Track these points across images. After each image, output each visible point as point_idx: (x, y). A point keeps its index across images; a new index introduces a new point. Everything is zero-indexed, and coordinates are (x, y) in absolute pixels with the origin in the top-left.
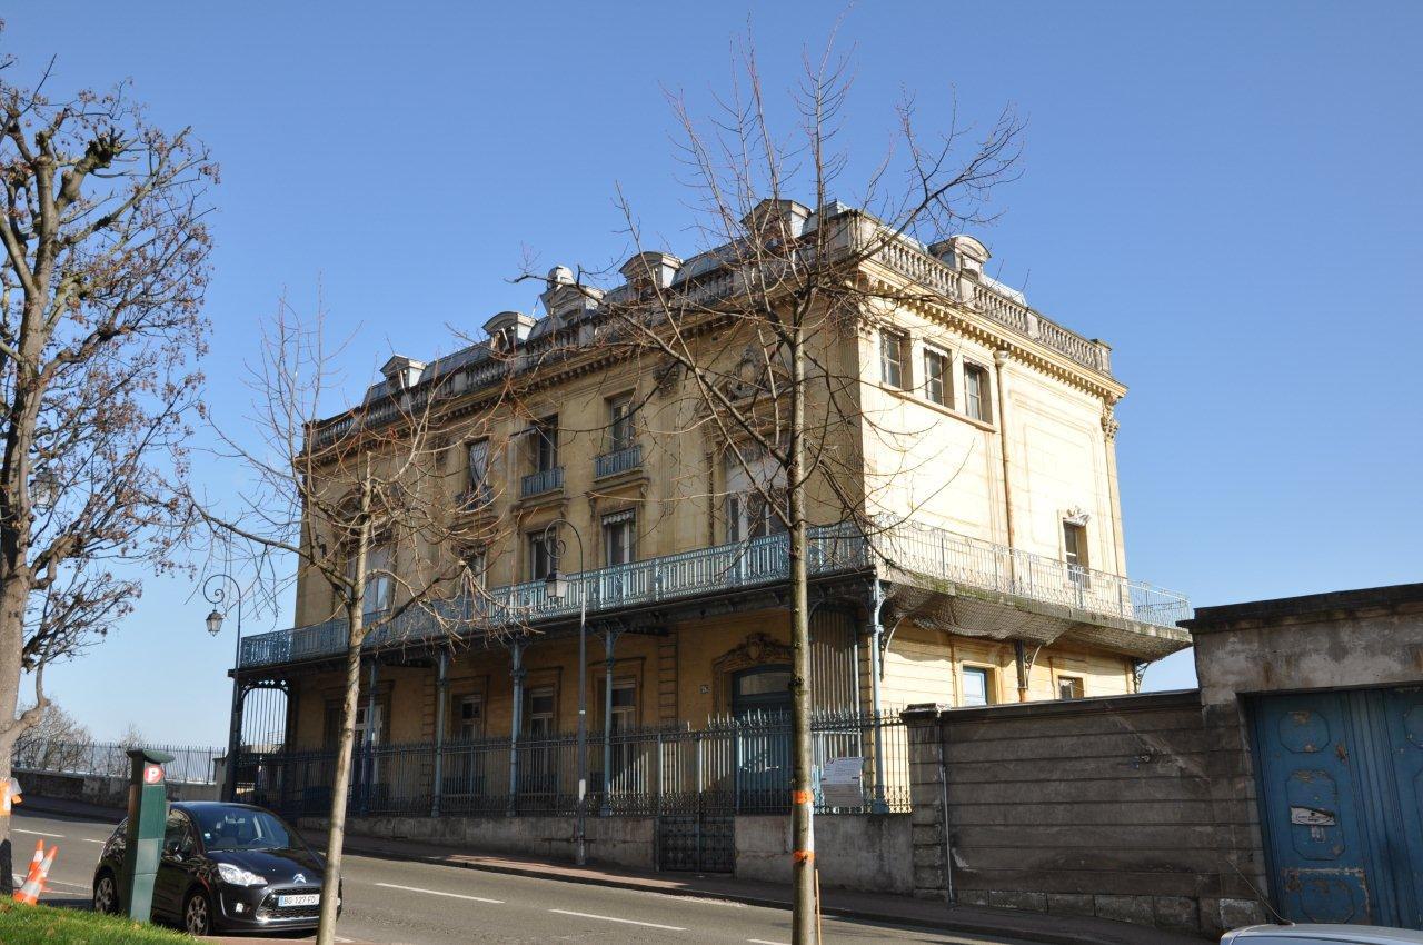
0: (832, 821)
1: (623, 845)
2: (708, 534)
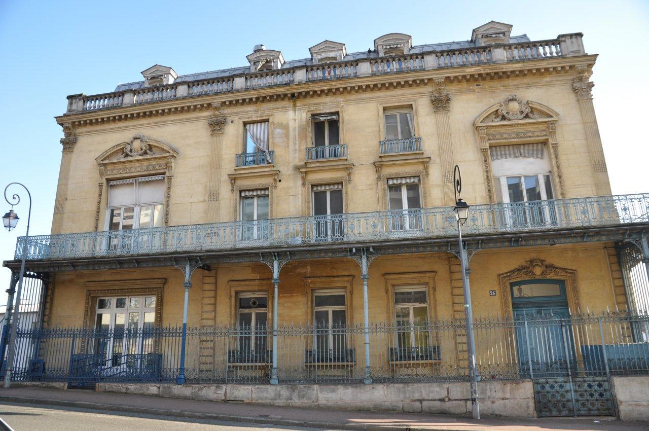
1: (503, 402)
2: (488, 197)
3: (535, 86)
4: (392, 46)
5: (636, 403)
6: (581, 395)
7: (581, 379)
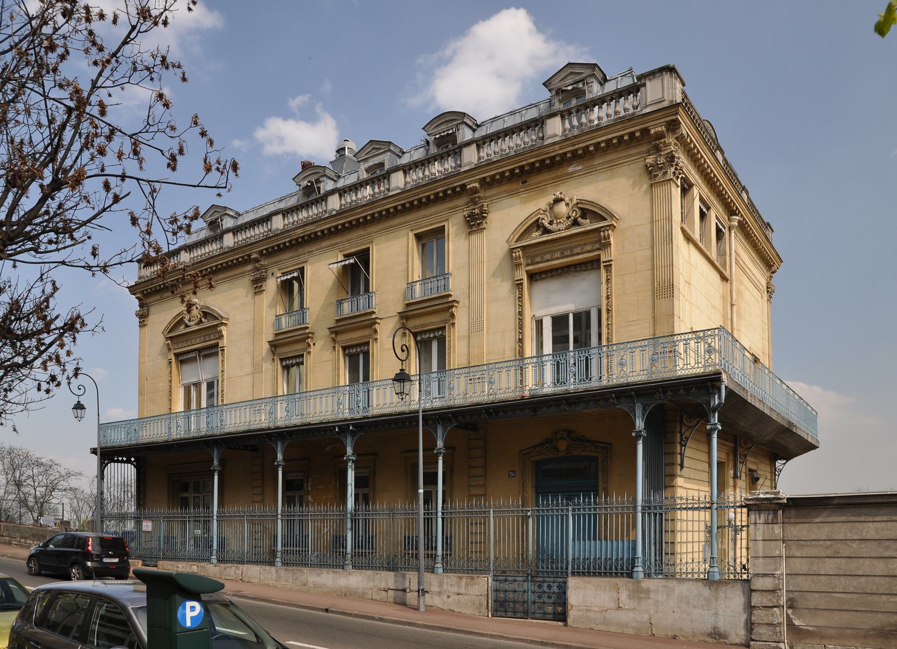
0: (666, 584)
1: (457, 597)
3: (596, 170)
4: (442, 134)
5: (587, 608)
6: (540, 597)
7: (541, 579)
